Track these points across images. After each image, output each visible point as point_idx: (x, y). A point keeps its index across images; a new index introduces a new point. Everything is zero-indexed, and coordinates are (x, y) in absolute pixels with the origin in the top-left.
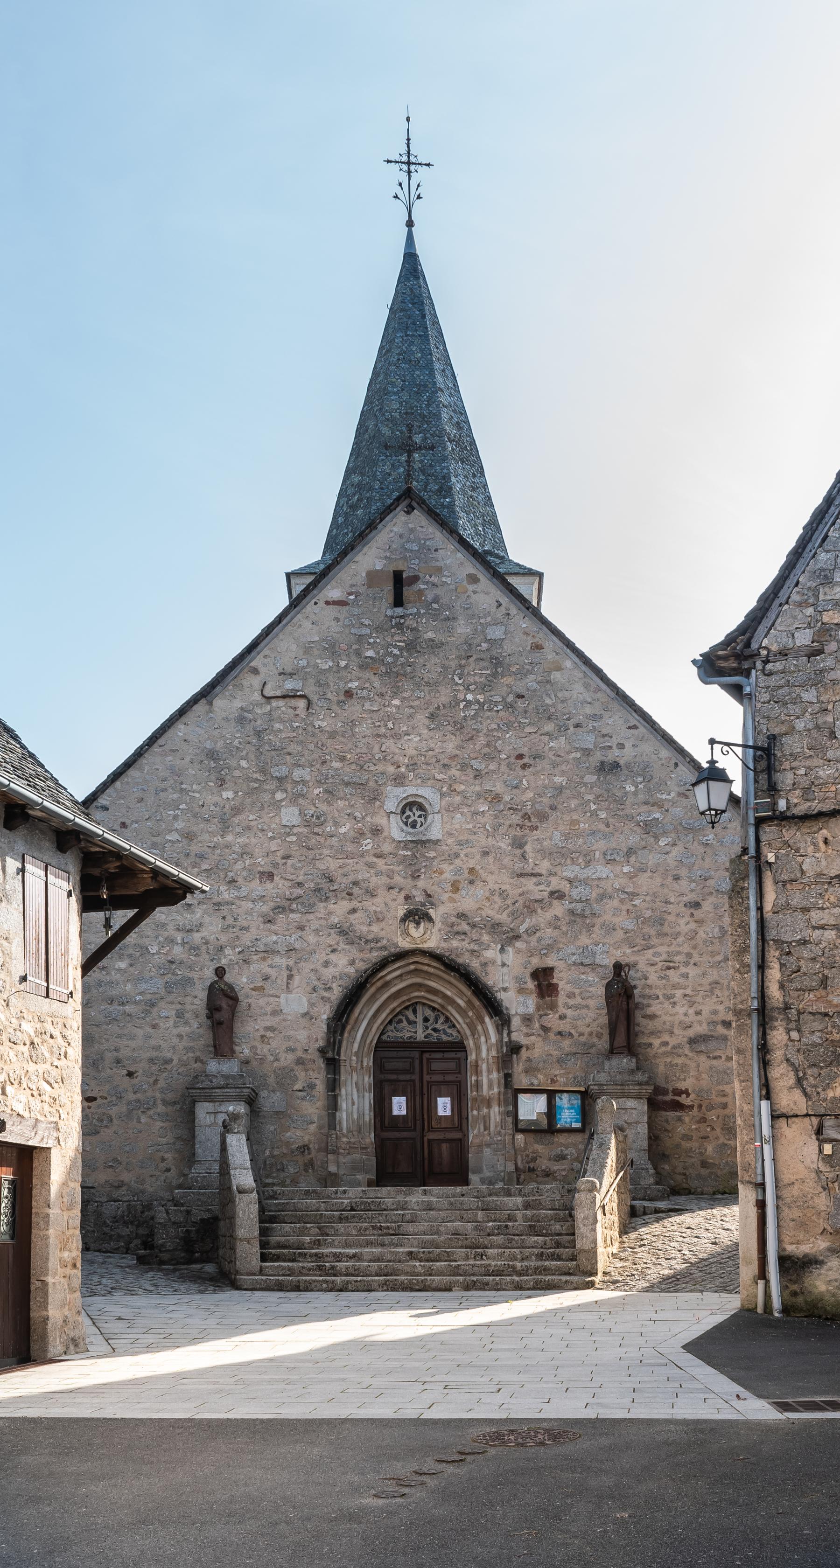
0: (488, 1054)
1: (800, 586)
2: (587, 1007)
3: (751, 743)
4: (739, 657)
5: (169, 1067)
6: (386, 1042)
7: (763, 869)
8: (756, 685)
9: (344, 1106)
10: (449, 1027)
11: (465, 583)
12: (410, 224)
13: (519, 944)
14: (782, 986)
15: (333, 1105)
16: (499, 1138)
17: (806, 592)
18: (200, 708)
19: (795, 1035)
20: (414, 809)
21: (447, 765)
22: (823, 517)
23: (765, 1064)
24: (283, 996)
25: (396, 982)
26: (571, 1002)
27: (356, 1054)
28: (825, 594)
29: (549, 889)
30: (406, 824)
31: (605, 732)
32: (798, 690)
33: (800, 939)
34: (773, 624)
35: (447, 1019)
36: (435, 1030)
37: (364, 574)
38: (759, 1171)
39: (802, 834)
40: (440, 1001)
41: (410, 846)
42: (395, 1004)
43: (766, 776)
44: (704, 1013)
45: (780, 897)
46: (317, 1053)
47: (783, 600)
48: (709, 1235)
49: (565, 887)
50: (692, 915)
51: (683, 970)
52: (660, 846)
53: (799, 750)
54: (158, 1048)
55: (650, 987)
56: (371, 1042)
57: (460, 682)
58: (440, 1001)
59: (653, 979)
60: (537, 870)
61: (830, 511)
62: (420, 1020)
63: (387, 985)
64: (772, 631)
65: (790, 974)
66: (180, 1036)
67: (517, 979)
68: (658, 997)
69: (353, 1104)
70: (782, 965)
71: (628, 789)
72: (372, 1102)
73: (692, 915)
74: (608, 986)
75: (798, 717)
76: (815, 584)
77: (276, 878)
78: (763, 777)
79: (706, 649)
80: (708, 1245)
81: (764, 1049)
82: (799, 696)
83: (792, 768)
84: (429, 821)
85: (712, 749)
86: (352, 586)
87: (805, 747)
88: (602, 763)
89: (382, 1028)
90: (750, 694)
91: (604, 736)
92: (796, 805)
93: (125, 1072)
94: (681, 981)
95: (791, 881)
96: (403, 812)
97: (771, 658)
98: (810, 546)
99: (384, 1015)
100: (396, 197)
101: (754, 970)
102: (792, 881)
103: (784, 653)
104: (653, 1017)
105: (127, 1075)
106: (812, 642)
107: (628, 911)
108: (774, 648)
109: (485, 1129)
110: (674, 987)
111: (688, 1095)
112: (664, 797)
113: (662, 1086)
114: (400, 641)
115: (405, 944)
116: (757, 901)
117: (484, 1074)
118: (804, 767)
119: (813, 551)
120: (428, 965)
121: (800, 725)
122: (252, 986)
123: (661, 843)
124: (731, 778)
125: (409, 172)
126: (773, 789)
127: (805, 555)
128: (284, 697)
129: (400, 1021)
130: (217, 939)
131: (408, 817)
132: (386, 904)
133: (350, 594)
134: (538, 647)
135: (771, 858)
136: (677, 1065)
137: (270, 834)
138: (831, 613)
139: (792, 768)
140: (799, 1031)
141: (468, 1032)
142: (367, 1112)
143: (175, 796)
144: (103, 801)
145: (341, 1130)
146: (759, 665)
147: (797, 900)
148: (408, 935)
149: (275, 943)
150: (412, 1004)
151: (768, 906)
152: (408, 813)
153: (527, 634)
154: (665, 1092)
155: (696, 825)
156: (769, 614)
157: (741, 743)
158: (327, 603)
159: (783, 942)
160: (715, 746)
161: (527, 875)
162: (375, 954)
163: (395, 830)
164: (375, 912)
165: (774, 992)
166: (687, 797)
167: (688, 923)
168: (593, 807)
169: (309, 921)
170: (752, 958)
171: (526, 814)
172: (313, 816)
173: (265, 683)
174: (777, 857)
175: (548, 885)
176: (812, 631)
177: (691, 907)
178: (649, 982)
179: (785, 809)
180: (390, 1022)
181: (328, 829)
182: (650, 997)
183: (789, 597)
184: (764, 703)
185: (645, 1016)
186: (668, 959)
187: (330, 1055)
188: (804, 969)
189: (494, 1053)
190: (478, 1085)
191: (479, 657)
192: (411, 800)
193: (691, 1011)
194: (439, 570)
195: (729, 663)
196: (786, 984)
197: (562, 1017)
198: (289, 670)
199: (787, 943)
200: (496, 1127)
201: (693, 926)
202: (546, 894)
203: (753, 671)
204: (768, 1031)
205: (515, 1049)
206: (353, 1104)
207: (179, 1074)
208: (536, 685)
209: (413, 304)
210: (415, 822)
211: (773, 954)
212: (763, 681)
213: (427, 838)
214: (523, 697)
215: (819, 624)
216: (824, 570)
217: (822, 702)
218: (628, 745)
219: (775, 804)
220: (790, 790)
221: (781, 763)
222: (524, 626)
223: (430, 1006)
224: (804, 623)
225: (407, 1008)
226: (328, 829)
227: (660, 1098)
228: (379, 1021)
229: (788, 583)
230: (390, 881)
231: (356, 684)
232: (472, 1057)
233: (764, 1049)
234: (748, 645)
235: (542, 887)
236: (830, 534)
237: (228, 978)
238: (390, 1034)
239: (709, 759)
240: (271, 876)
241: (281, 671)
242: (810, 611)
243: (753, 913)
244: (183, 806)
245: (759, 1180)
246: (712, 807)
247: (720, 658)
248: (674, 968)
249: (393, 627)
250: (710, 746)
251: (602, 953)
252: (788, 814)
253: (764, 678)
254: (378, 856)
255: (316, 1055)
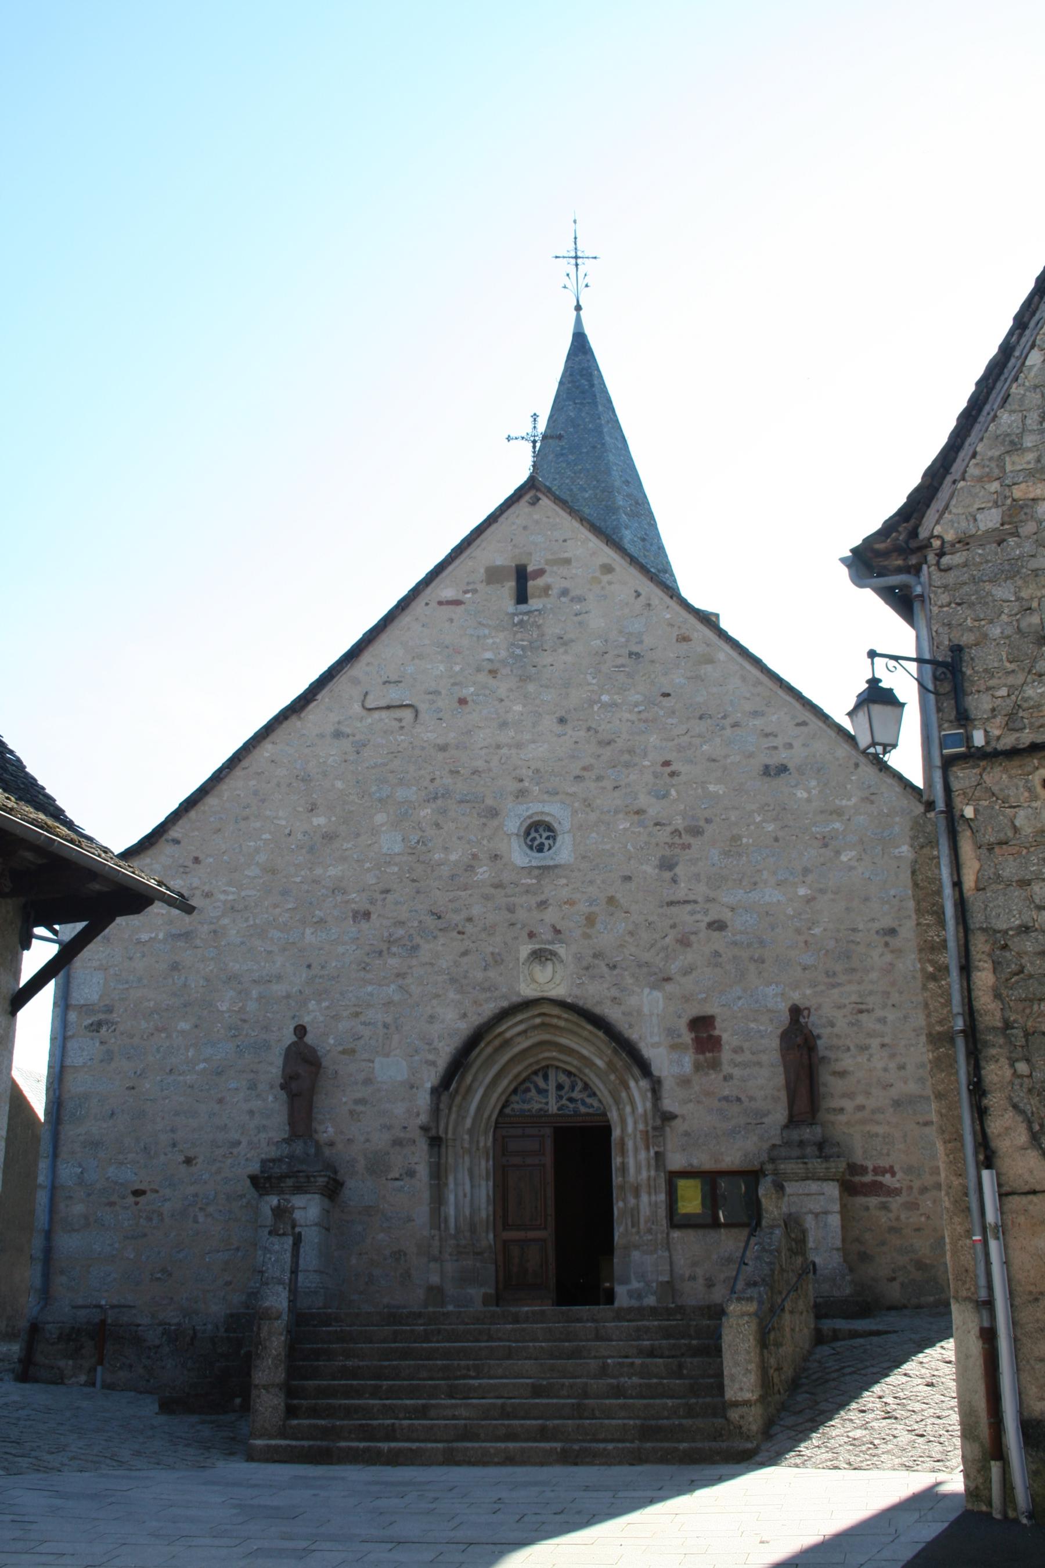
0: (635, 1128)
1: (978, 457)
2: (759, 1064)
3: (927, 656)
4: (904, 551)
5: (235, 1151)
6: (509, 1116)
7: (959, 829)
8: (930, 585)
9: (452, 1198)
10: (589, 1096)
11: (598, 574)
12: (578, 308)
13: (669, 987)
14: (998, 996)
15: (438, 1199)
16: (650, 1237)
17: (987, 463)
18: (294, 723)
19: (1022, 1067)
20: (541, 830)
21: (579, 777)
22: (1001, 373)
23: (980, 1113)
24: (377, 1060)
25: (519, 1039)
26: (739, 1058)
27: (470, 1132)
28: (1013, 463)
29: (707, 919)
30: (531, 848)
31: (768, 730)
32: (988, 586)
33: (1020, 926)
34: (947, 507)
35: (586, 1086)
36: (571, 1100)
37: (482, 570)
38: (982, 1281)
39: (1010, 777)
40: (575, 1062)
41: (536, 872)
42: (519, 1068)
43: (953, 702)
44: (908, 1067)
45: (986, 867)
46: (418, 1131)
47: (958, 476)
48: (923, 1371)
49: (727, 915)
50: (887, 944)
51: (879, 1013)
52: (842, 862)
53: (996, 665)
54: (225, 1128)
55: (838, 1036)
56: (490, 1117)
57: (594, 681)
58: (575, 1062)
59: (841, 1025)
60: (692, 897)
61: (1010, 365)
62: (552, 1086)
63: (507, 1043)
64: (946, 515)
65: (1011, 976)
66: (251, 1112)
67: (671, 1032)
68: (848, 1049)
69: (465, 1196)
70: (997, 966)
71: (799, 795)
72: (491, 1193)
73: (887, 944)
74: (785, 1036)
75: (991, 622)
76: (997, 453)
77: (374, 917)
78: (948, 705)
79: (857, 542)
80: (921, 1387)
81: (978, 1090)
82: (989, 593)
83: (988, 689)
84: (558, 844)
85: (873, 663)
86: (468, 584)
87: (1004, 657)
88: (767, 767)
89: (504, 1098)
90: (922, 596)
91: (767, 735)
92: (998, 738)
93: (181, 1158)
94: (878, 1027)
95: (1001, 843)
96: (527, 833)
97: (947, 548)
98: (987, 408)
99: (505, 1083)
100: (565, 287)
101: (955, 973)
102: (1001, 843)
103: (964, 541)
104: (842, 1074)
105: (184, 1162)
106: (1002, 525)
107: (806, 942)
108: (949, 537)
109: (633, 1226)
110: (869, 1035)
111: (893, 1174)
112: (844, 802)
113: (859, 1163)
114: (523, 640)
115: (527, 991)
116: (952, 875)
117: (631, 1153)
118: (1005, 685)
119: (992, 414)
120: (559, 1017)
121: (996, 631)
122: (340, 1048)
123: (844, 858)
124: (902, 700)
125: (577, 265)
126: (964, 718)
127: (981, 419)
128: (388, 707)
129: (528, 1090)
130: (300, 992)
131: (533, 839)
132: (506, 944)
133: (466, 592)
134: (684, 639)
135: (969, 812)
136: (877, 1135)
137: (367, 865)
138: (1023, 486)
139: (988, 689)
140: (1028, 1061)
141: (610, 1100)
142: (483, 1206)
143: (258, 825)
144: (174, 833)
145: (447, 1228)
146: (931, 558)
147: (1010, 869)
148: (534, 981)
149: (371, 994)
150: (543, 1068)
151: (969, 881)
152: (533, 834)
153: (672, 626)
154: (864, 1170)
155: (885, 834)
156: (939, 495)
157: (914, 656)
158: (440, 603)
159: (996, 931)
160: (877, 660)
161: (679, 902)
162: (492, 1005)
163: (519, 855)
164: (492, 954)
165: (984, 1001)
166: (872, 802)
167: (882, 955)
168: (758, 819)
169: (410, 967)
170: (951, 958)
171: (676, 830)
172: (418, 842)
173: (367, 693)
174: (976, 811)
175: (706, 912)
176: (1000, 510)
177: (885, 934)
178: (836, 1030)
179: (983, 743)
180: (515, 1091)
181: (437, 856)
182: (838, 1048)
183: (965, 472)
184: (942, 607)
185: (835, 1073)
186: (859, 1000)
187: (433, 1133)
188: (1029, 968)
189: (641, 1127)
190: (624, 1169)
191: (616, 652)
192: (536, 818)
193: (892, 1065)
194: (567, 561)
195: (893, 560)
196: (1004, 992)
197: (728, 1078)
198: (394, 677)
199: (999, 932)
200: (646, 1222)
201: (889, 957)
202: (703, 925)
203: (925, 567)
204: (983, 1063)
205: (668, 1117)
206: (465, 1196)
207: (247, 1160)
208: (683, 681)
209: (582, 376)
210: (542, 844)
211: (980, 945)
212: (938, 578)
213: (556, 862)
214: (668, 695)
215: (1009, 501)
216: (1008, 435)
217: (1023, 599)
218: (797, 744)
219: (969, 738)
220: (988, 719)
221: (973, 683)
222: (668, 616)
223: (565, 1071)
224: (989, 501)
225: (536, 1073)
226: (437, 856)
227: (857, 1179)
228: (500, 1090)
229: (962, 454)
230: (510, 916)
231: (472, 689)
232: (616, 1133)
233: (978, 1090)
234: (914, 534)
235: (698, 917)
236: (1013, 390)
237: (309, 1039)
238: (516, 1106)
239: (870, 676)
240: (367, 915)
241: (386, 679)
242: (995, 486)
243: (948, 891)
244: (267, 836)
245: (983, 1294)
246: (878, 739)
247: (879, 554)
248: (868, 1011)
249: (516, 625)
250: (869, 660)
251: (776, 995)
252: (989, 749)
253: (939, 574)
254: (496, 886)
255: (417, 1134)
